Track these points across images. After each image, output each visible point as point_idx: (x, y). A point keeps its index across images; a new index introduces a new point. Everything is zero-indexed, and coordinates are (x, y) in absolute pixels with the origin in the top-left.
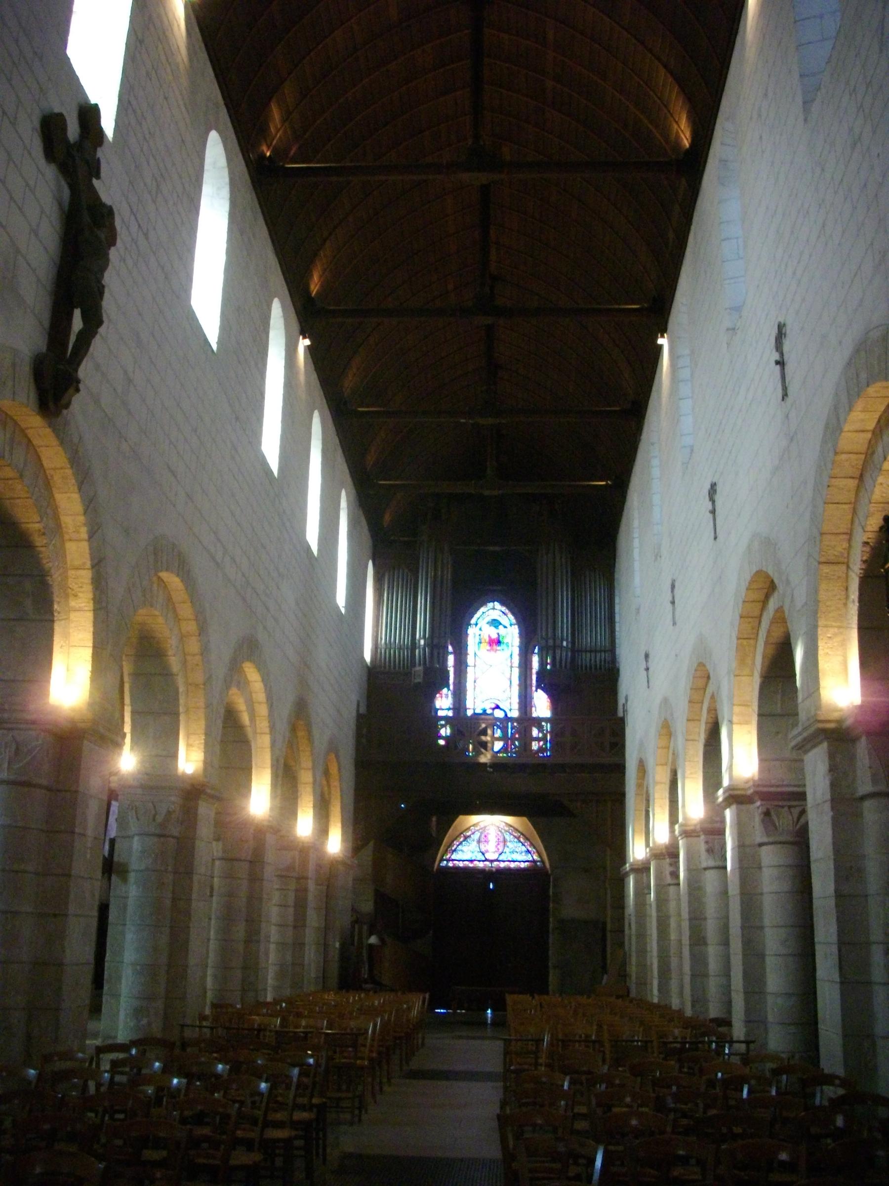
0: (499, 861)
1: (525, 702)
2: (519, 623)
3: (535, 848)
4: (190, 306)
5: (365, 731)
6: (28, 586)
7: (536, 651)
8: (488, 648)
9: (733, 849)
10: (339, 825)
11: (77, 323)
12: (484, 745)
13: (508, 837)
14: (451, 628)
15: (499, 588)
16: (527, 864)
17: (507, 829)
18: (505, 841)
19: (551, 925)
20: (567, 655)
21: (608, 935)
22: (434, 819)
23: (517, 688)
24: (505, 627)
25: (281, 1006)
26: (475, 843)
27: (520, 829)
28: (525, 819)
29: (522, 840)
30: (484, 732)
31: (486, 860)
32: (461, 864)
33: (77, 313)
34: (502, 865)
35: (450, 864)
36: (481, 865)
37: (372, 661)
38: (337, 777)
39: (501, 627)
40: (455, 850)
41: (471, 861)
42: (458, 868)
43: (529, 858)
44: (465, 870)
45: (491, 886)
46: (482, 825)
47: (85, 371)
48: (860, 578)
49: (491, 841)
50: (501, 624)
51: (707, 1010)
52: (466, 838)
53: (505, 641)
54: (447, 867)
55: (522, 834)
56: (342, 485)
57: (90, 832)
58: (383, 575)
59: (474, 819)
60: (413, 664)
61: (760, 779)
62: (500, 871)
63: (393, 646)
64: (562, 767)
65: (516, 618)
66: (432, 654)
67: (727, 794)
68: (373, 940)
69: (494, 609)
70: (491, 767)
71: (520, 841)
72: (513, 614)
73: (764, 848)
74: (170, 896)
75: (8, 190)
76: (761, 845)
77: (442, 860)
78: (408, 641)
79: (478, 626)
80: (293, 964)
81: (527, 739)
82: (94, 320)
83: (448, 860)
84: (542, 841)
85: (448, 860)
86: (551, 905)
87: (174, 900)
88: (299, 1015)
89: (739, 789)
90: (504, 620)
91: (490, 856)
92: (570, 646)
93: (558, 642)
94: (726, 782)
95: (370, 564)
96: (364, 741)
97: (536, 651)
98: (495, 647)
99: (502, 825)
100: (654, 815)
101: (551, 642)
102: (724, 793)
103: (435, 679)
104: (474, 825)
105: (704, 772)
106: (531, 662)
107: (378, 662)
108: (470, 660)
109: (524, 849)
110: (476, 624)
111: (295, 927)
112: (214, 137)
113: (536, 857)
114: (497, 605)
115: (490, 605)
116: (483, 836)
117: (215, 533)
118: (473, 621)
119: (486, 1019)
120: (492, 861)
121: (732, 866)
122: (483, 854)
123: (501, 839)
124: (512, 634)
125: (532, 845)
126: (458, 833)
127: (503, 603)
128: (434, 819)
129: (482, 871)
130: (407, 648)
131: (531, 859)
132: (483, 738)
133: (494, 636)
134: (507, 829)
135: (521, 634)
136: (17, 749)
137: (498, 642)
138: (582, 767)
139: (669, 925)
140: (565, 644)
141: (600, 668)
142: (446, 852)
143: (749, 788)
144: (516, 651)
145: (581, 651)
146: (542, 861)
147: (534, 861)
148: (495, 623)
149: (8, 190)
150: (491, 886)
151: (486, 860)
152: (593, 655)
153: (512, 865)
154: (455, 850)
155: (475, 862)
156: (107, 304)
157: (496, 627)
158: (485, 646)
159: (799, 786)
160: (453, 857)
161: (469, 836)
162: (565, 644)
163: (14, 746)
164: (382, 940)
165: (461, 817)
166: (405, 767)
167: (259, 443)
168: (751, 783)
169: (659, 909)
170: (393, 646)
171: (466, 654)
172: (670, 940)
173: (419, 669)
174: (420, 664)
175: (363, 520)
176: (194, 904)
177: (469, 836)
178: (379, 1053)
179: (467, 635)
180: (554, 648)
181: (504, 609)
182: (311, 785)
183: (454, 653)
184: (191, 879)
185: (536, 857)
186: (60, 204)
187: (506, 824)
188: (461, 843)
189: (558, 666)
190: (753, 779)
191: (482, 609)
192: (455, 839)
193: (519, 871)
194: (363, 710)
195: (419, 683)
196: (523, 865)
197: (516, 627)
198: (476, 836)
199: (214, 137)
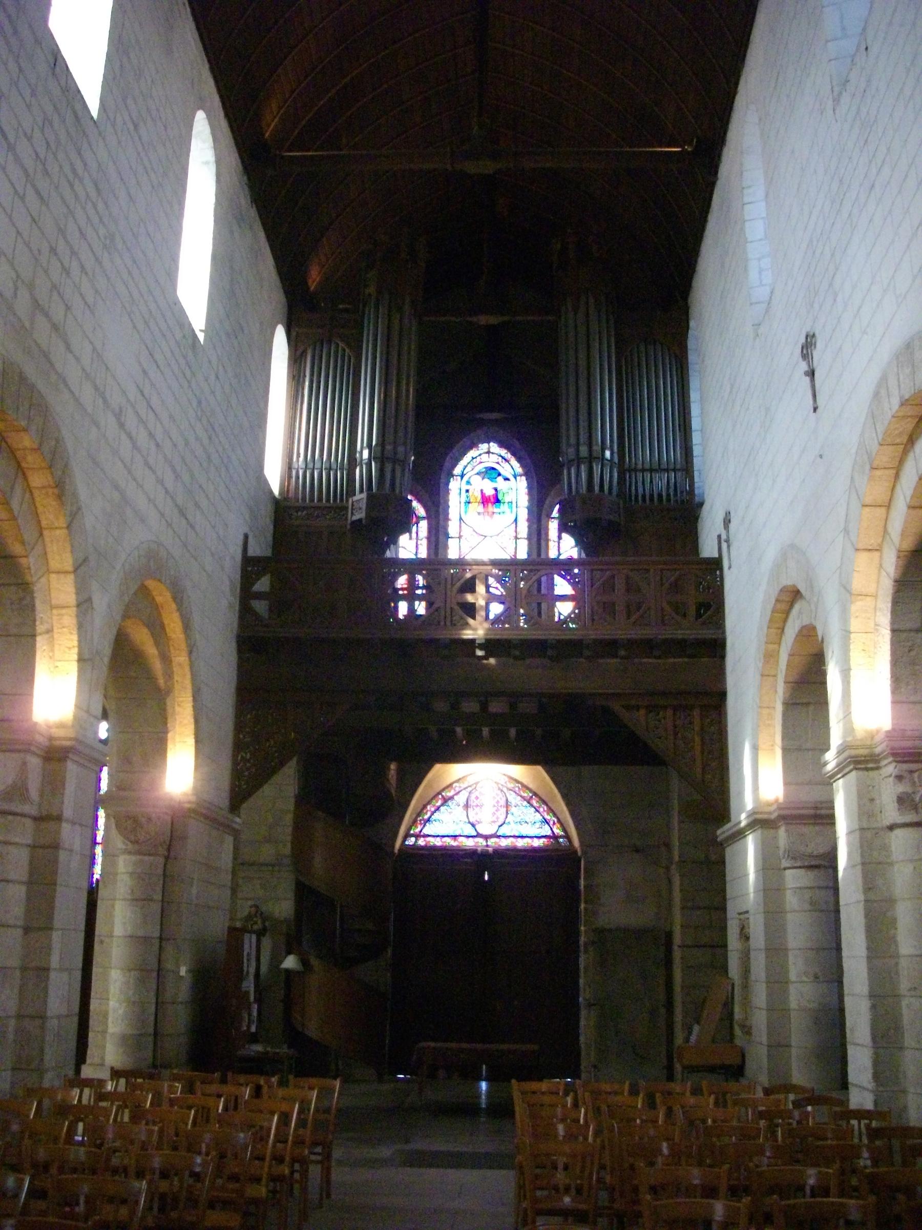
0: (499, 837)
1: (538, 536)
2: (526, 474)
3: (555, 815)
4: (177, 303)
7: (555, 513)
8: (480, 508)
9: (850, 833)
10: (191, 741)
12: (471, 610)
13: (513, 799)
14: (418, 467)
15: (495, 416)
16: (542, 840)
17: (511, 785)
18: (507, 805)
19: (582, 939)
20: (611, 477)
21: (677, 954)
22: (393, 766)
23: (526, 524)
24: (507, 479)
26: (461, 809)
27: (531, 786)
28: (539, 768)
29: (535, 804)
30: (470, 586)
31: (479, 835)
32: (438, 842)
34: (504, 843)
35: (421, 842)
36: (469, 843)
37: (280, 494)
38: (183, 646)
39: (500, 479)
40: (428, 820)
41: (455, 837)
42: (434, 848)
43: (546, 831)
44: (444, 849)
45: (486, 878)
46: (470, 781)
48: (896, 581)
49: (485, 804)
50: (499, 475)
52: (445, 801)
53: (507, 499)
54: (414, 847)
55: (535, 794)
58: (304, 354)
59: (454, 771)
60: (351, 492)
61: (785, 801)
62: (500, 853)
63: (318, 465)
64: (610, 647)
65: (523, 466)
66: (381, 471)
67: (751, 819)
68: (290, 962)
69: (488, 452)
70: (481, 647)
71: (532, 806)
72: (519, 460)
73: (898, 832)
75: (14, 225)
76: (891, 828)
77: (407, 835)
78: (342, 456)
79: (466, 478)
80: (20, 1017)
81: (542, 598)
83: (417, 836)
84: (568, 804)
85: (417, 836)
86: (583, 906)
89: (761, 813)
90: (505, 470)
91: (484, 829)
92: (616, 460)
93: (597, 448)
94: (749, 804)
95: (280, 338)
96: (260, 607)
97: (555, 513)
98: (490, 508)
99: (503, 780)
100: (846, 673)
101: (584, 451)
102: (748, 817)
103: (390, 519)
104: (458, 781)
105: (895, 631)
106: (547, 529)
107: (291, 494)
108: (453, 528)
109: (538, 817)
110: (462, 476)
111: (27, 930)
112: (200, 116)
113: (558, 831)
114: (494, 447)
115: (484, 447)
116: (473, 797)
117: (172, 498)
118: (457, 470)
119: (479, 1096)
120: (486, 838)
121: (850, 854)
122: (473, 825)
123: (503, 802)
124: (517, 491)
125: (551, 810)
126: (432, 794)
127: (502, 445)
128: (393, 766)
129: (472, 853)
130: (342, 469)
131: (549, 833)
132: (470, 598)
133: (489, 492)
134: (511, 785)
135: (530, 488)
137: (497, 501)
138: (648, 646)
139: (894, 921)
140: (608, 454)
141: (669, 500)
142: (414, 823)
143: (774, 811)
144: (523, 514)
145: (636, 470)
146: (567, 836)
147: (555, 837)
148: (491, 473)
149: (14, 225)
150: (486, 878)
151: (479, 835)
152: (656, 476)
153: (520, 843)
154: (428, 820)
155: (461, 839)
157: (492, 479)
158: (477, 507)
159: (827, 808)
160: (426, 831)
161: (452, 798)
162: (608, 454)
164: (304, 962)
165: (438, 767)
166: (327, 661)
167: (175, 290)
168: (775, 807)
169: (869, 886)
171: (447, 519)
172: (896, 956)
173: (360, 497)
174: (361, 491)
177: (452, 798)
179: (447, 491)
180: (591, 459)
181: (503, 452)
182: (73, 611)
183: (428, 518)
185: (558, 831)
187: (511, 778)
188: (438, 809)
189: (597, 488)
190: (777, 801)
191: (472, 453)
192: (429, 803)
193: (531, 854)
195: (360, 520)
196: (537, 843)
197: (524, 478)
198: (461, 799)
199: (200, 116)
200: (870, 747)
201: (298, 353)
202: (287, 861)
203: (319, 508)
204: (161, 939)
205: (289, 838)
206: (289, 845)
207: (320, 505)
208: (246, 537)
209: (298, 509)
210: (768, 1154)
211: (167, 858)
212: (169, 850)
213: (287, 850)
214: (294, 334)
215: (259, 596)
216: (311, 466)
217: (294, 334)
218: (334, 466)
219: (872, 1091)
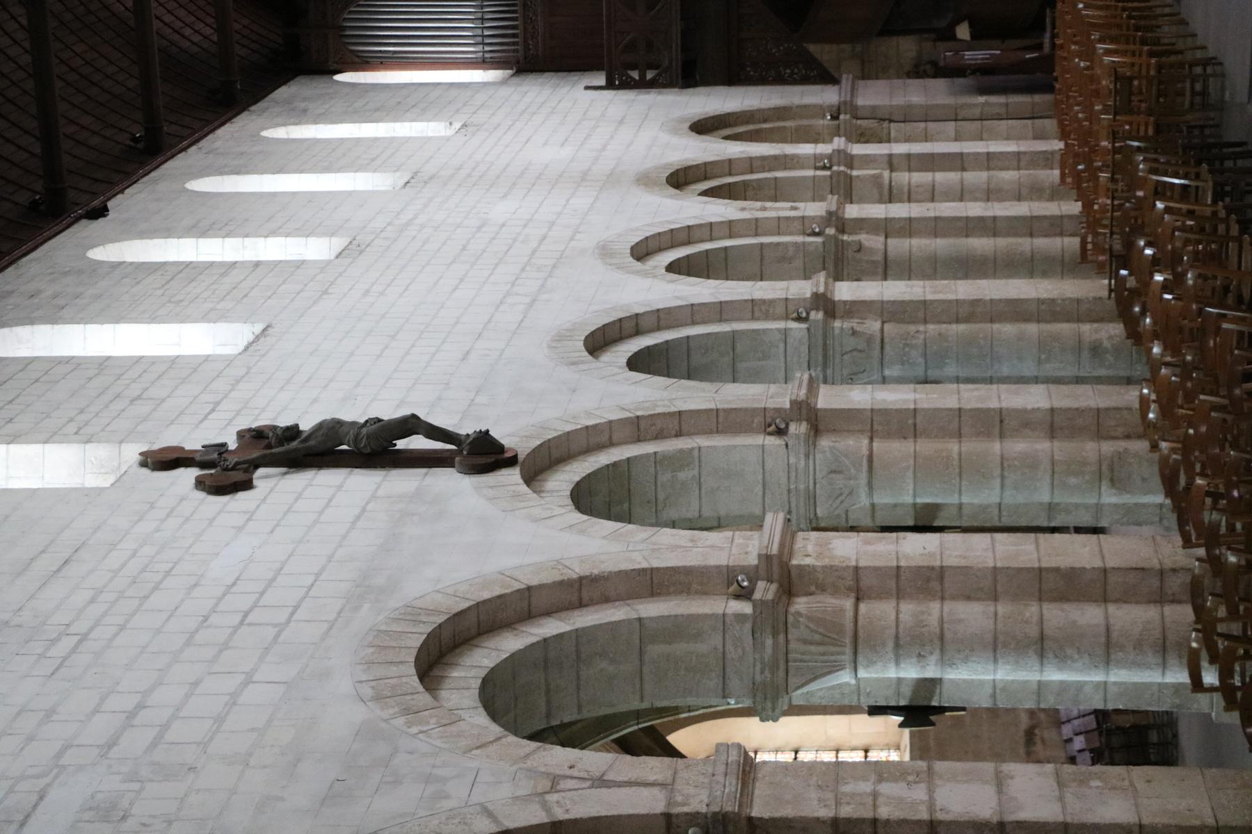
5: (635, 75)
6: (665, 477)
11: (418, 443)
25: (1082, 171)
33: (401, 444)
47: (467, 428)
51: (1070, 217)
56: (256, 138)
57: (911, 396)
74: (954, 326)
82: (411, 425)
87: (958, 321)
88: (1094, 150)
95: (338, 77)
96: (650, 75)
112: (265, 133)
130: (482, 7)
136: (834, 472)
156: (389, 411)
163: (833, 475)
170: (479, 32)
175: (283, 92)
176: (961, 297)
178: (1144, 42)
184: (932, 302)
186: (286, 473)
194: (601, 80)
200: (1017, 662)
201: (357, 60)
202: (859, 48)
203: (525, 28)
204: (956, 120)
205: (835, 47)
206: (843, 46)
207: (521, 27)
208: (587, 88)
209: (527, 48)
210: (1217, 451)
211: (891, 121)
212: (884, 120)
213: (847, 47)
214: (339, 67)
215: (643, 76)
216: (479, 39)
217: (335, 66)
218: (479, 15)
219: (1147, 431)
